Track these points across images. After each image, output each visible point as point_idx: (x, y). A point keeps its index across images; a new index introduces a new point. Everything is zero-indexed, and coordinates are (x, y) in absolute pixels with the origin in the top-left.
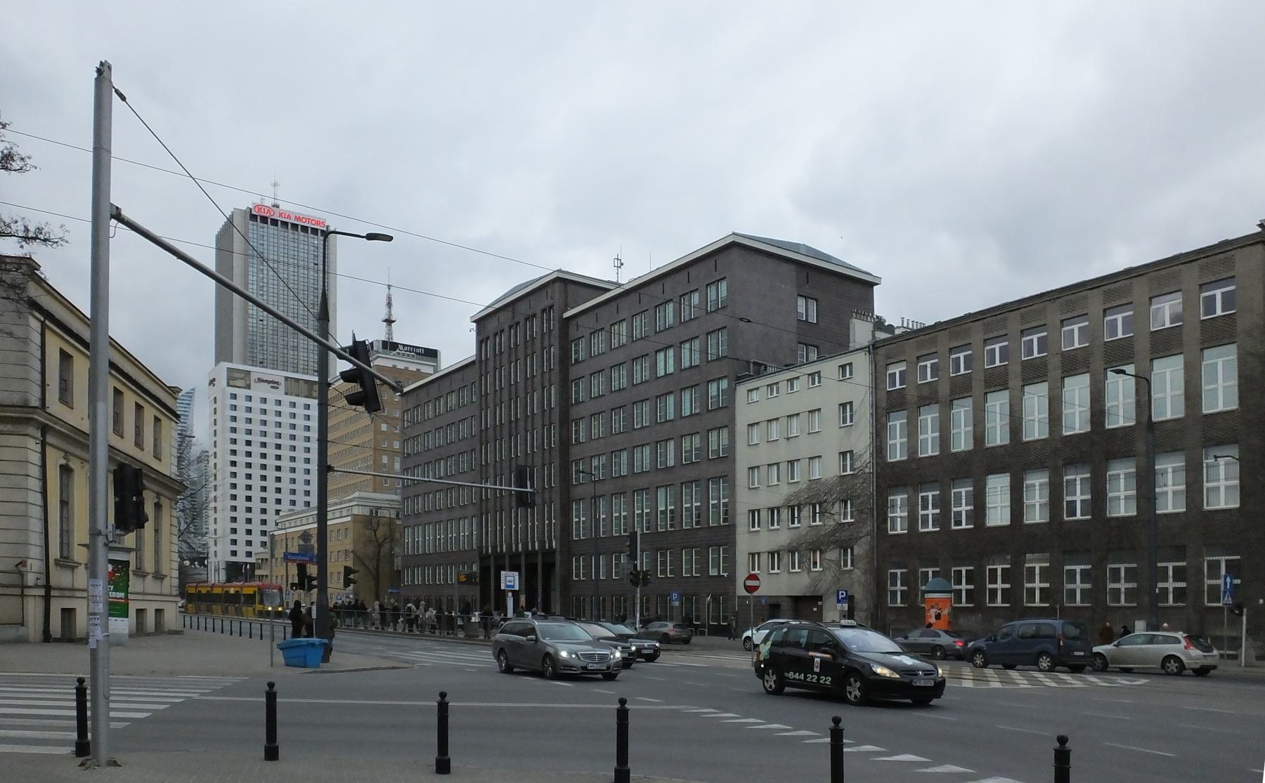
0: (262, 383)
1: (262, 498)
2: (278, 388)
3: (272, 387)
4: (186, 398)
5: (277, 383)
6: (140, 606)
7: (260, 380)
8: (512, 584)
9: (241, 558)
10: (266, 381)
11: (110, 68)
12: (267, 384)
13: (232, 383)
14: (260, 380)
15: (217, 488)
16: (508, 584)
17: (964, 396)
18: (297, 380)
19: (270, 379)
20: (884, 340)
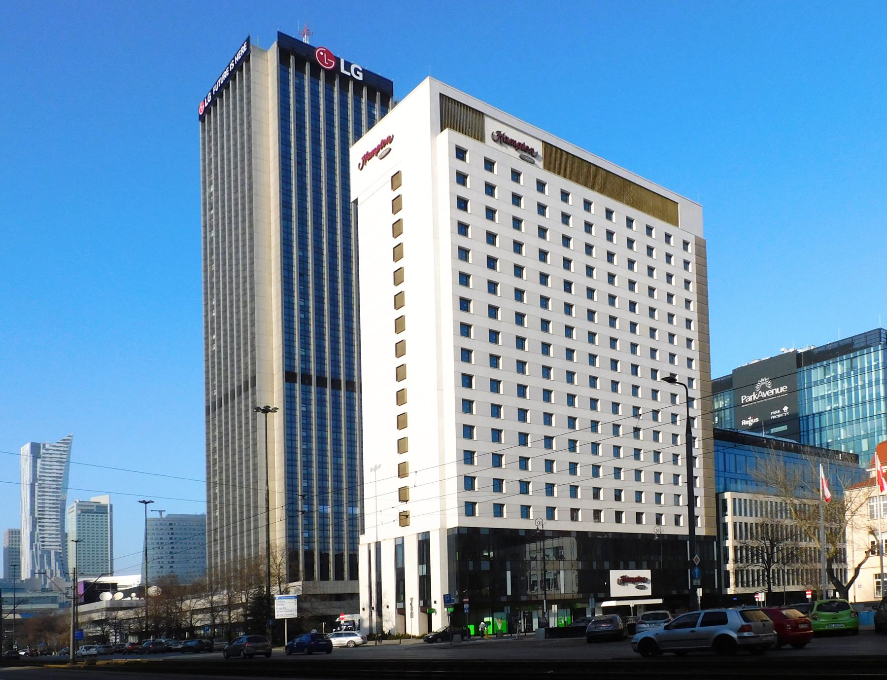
5: (531, 151)
9: (484, 520)
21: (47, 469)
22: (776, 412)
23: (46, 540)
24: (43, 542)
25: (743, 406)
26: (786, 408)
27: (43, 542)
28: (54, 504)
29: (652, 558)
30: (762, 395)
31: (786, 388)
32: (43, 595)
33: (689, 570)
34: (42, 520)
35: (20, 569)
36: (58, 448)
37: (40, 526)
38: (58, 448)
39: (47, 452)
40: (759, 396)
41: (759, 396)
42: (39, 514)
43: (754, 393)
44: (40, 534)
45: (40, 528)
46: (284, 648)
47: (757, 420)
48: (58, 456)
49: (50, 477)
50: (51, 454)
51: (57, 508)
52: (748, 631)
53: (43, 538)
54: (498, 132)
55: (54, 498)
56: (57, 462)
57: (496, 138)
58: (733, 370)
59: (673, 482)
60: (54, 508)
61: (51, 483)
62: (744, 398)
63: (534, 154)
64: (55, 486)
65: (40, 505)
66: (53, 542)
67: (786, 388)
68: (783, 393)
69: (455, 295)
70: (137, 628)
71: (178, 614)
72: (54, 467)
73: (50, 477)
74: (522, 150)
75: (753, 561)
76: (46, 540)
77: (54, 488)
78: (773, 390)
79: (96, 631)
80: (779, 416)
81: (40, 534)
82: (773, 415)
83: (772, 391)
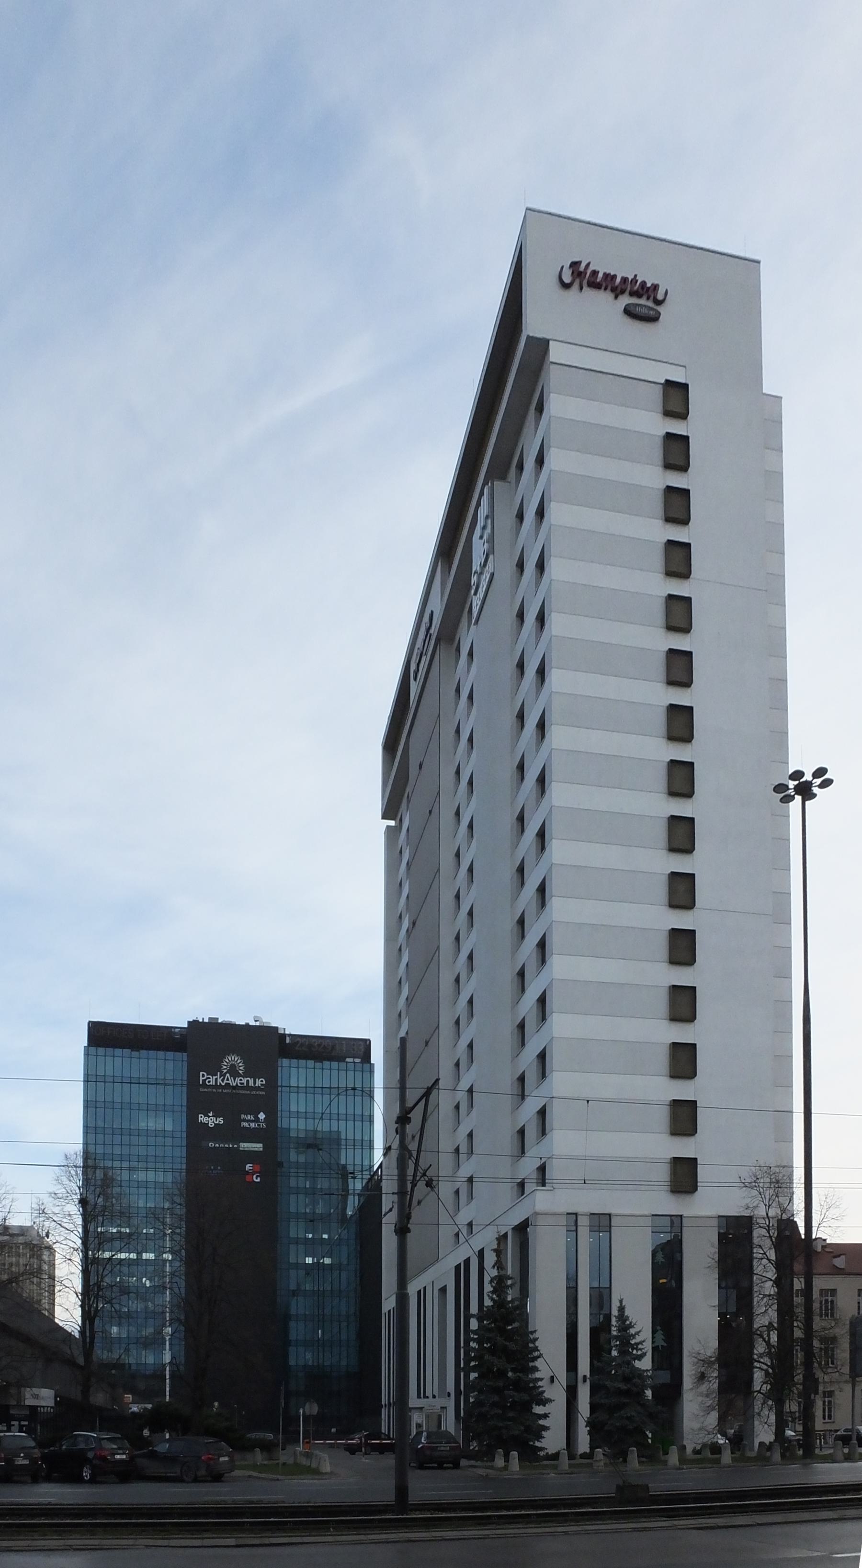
0: (588, 292)
22: (249, 1117)
25: (201, 1090)
26: (262, 1116)
29: (618, 1347)
30: (230, 1082)
31: (264, 1083)
40: (225, 1081)
41: (225, 1081)
43: (219, 1073)
46: (796, 796)
47: (220, 1121)
54: (575, 265)
57: (567, 279)
58: (189, 1022)
59: (794, 1114)
62: (203, 1076)
63: (660, 297)
67: (264, 1083)
68: (258, 1088)
69: (781, 553)
70: (166, 1222)
71: (28, 1268)
74: (632, 294)
75: (827, 1315)
78: (246, 1079)
80: (252, 1125)
82: (245, 1120)
83: (244, 1081)
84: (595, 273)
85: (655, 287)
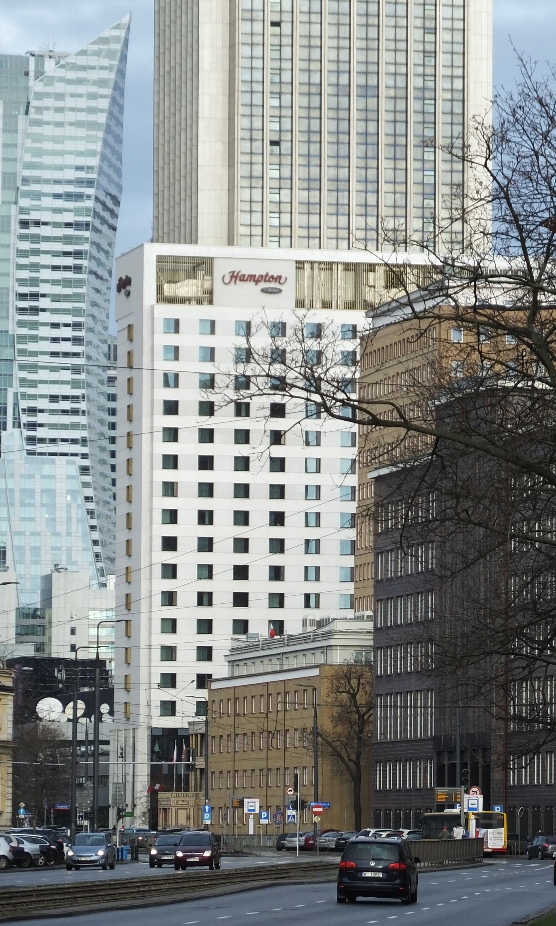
1: (200, 621)
2: (280, 291)
3: (264, 291)
4: (93, 61)
5: (278, 279)
6: (156, 711)
7: (236, 277)
8: (475, 806)
10: (253, 278)
11: (6, 571)
12: (252, 284)
13: (169, 290)
14: (236, 277)
15: (253, 330)
16: (470, 806)
17: (131, 774)
18: (328, 266)
19: (258, 272)
20: (159, 746)
21: (47, 239)
23: (40, 418)
24: (33, 426)
27: (33, 426)
28: (66, 283)
32: (198, 720)
33: (31, 669)
34: (31, 347)
35: (153, 752)
36: (82, 74)
37: (22, 367)
38: (82, 74)
39: (49, 89)
42: (21, 324)
44: (24, 396)
45: (24, 374)
48: (83, 103)
49: (57, 182)
50: (60, 96)
51: (78, 298)
52: (528, 337)
53: (32, 411)
55: (69, 261)
56: (78, 124)
57: (227, 279)
60: (66, 298)
61: (60, 203)
64: (70, 218)
65: (25, 290)
66: (64, 427)
72: (69, 146)
73: (57, 182)
74: (265, 281)
76: (40, 418)
77: (69, 182)
79: (514, 691)
81: (24, 396)
84: (244, 276)
85: (280, 277)
